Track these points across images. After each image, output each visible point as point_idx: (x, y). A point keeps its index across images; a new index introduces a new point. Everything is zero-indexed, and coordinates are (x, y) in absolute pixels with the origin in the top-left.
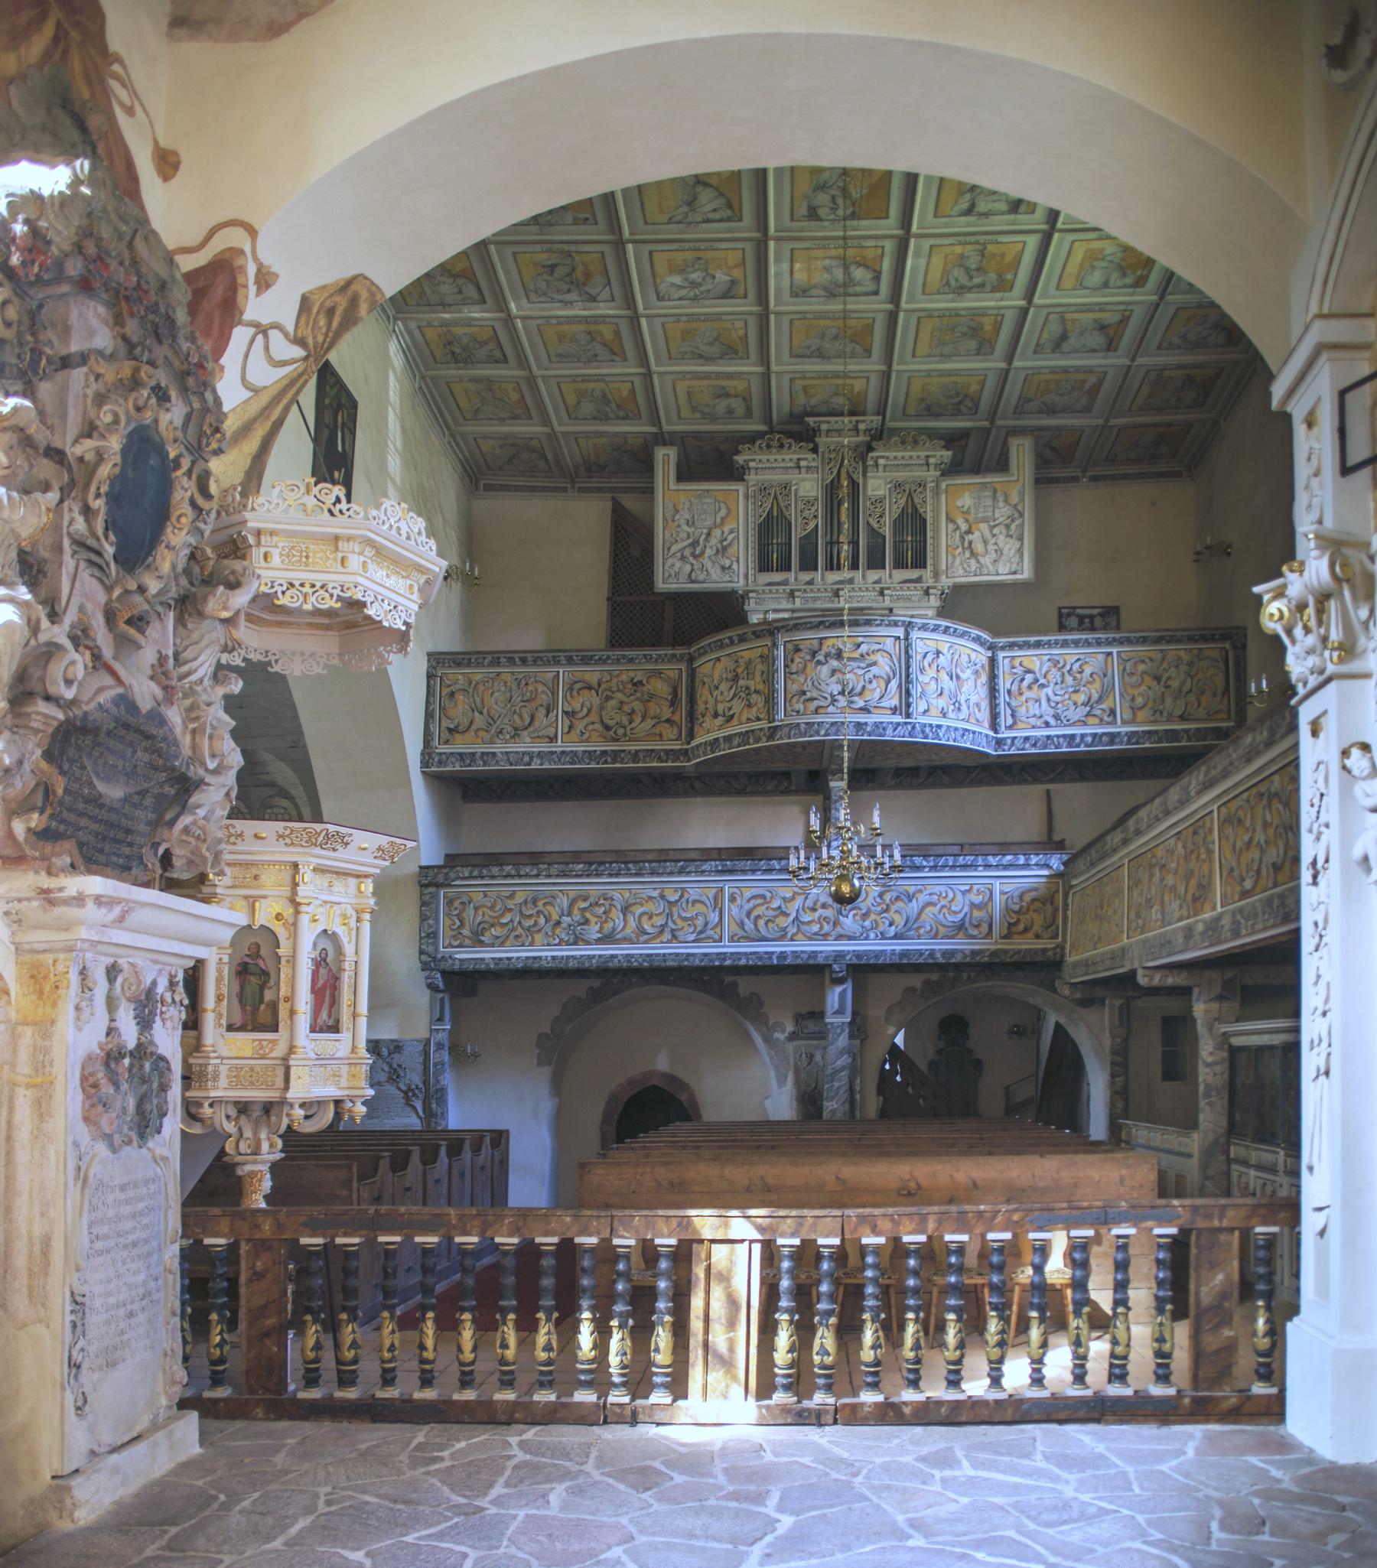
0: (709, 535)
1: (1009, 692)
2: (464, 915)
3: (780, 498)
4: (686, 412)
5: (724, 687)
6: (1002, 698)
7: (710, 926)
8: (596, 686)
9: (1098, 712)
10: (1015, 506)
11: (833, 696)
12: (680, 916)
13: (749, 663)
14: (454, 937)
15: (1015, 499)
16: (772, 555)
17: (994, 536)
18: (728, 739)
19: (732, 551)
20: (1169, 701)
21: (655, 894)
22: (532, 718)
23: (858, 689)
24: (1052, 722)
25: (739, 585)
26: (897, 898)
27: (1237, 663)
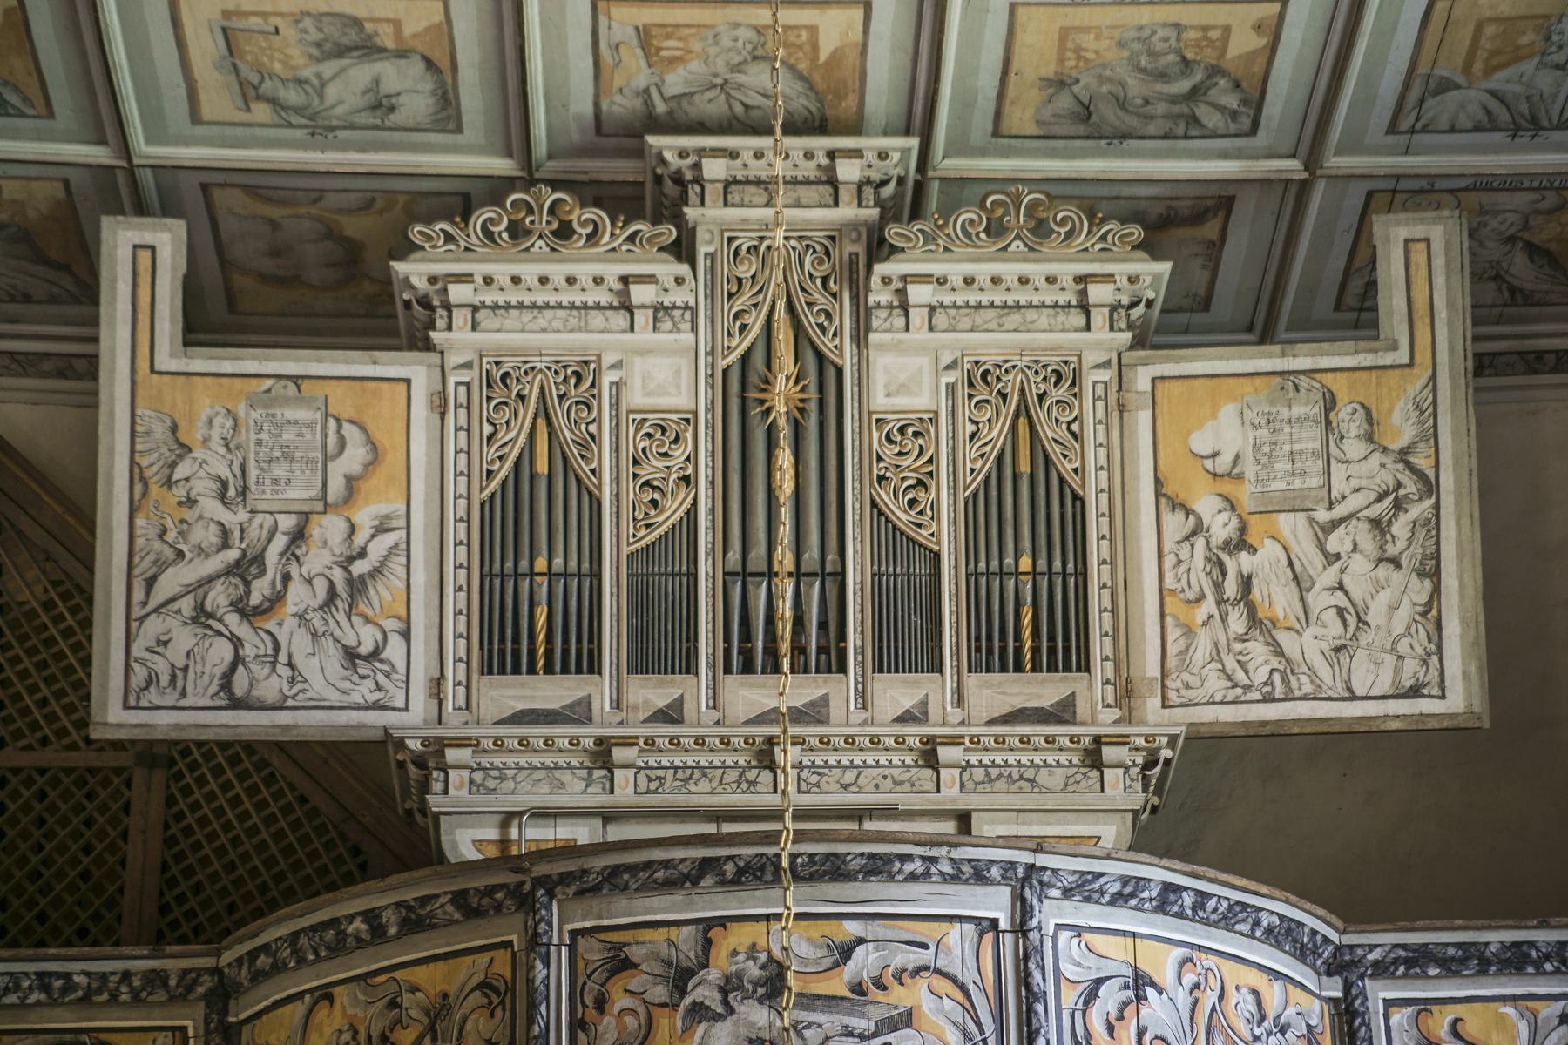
0: (299, 535)
3: (559, 412)
10: (1403, 456)
15: (1402, 428)
19: (384, 593)
25: (411, 718)
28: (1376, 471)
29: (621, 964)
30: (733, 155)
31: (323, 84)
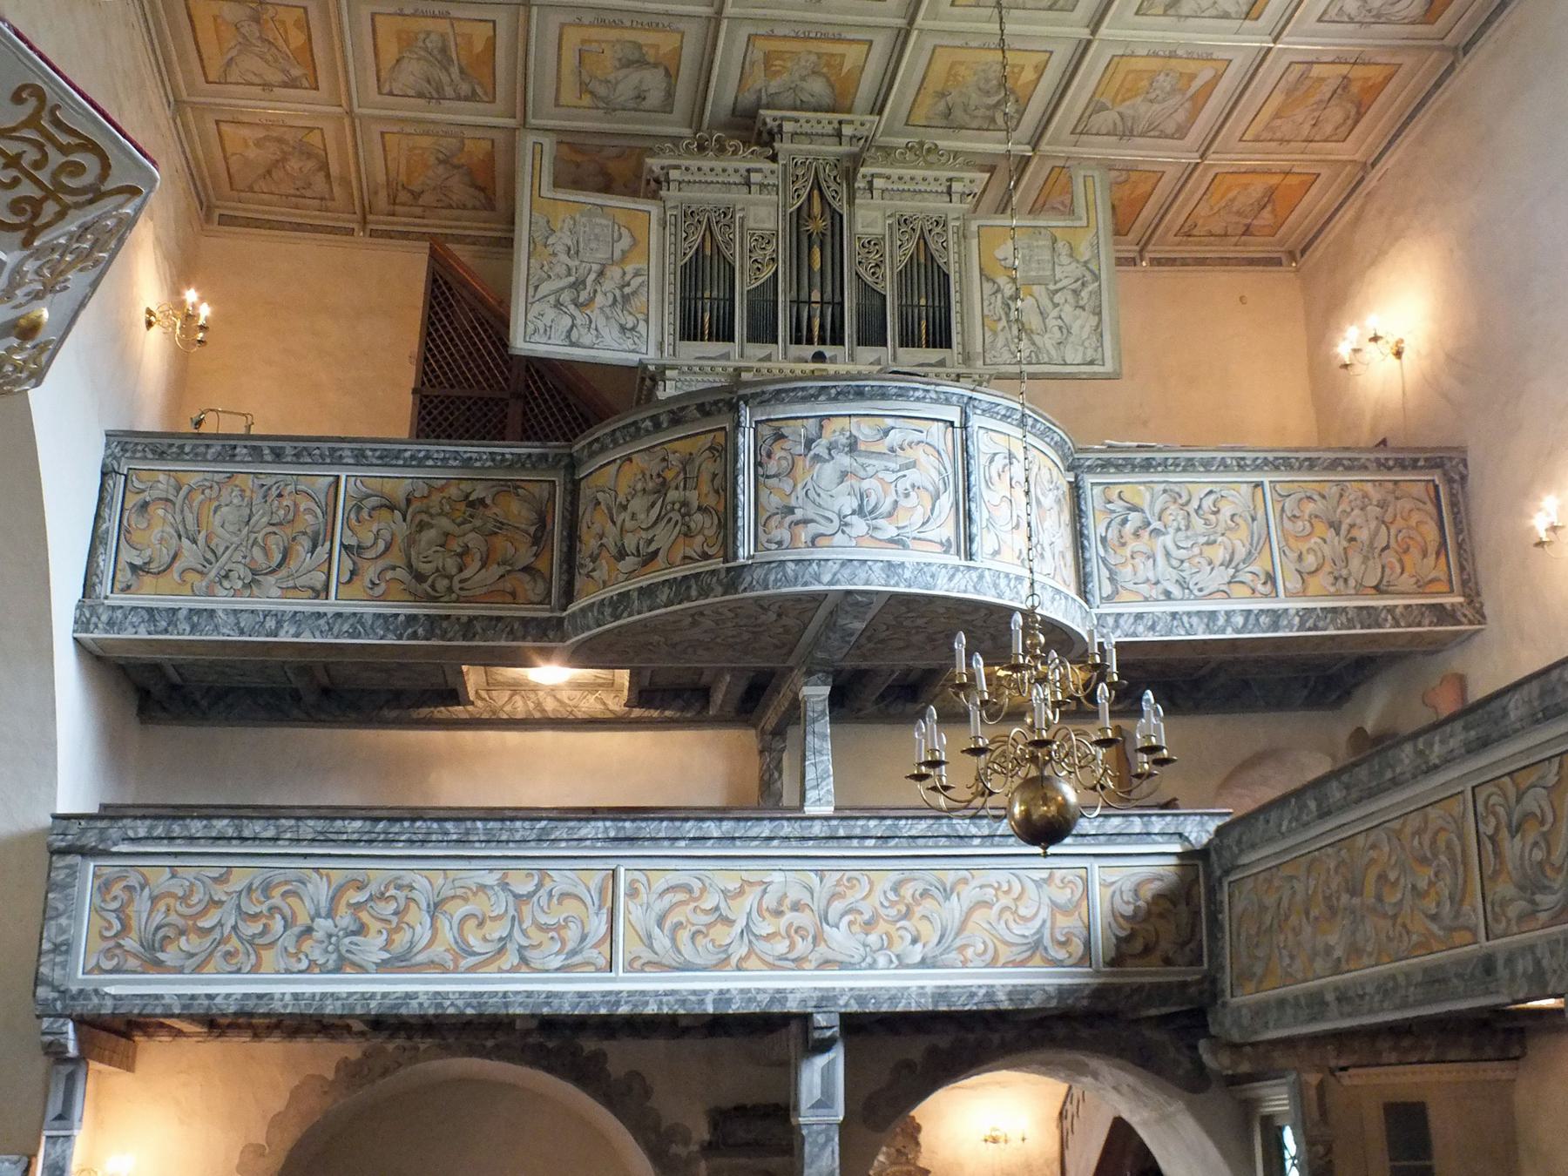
0: (601, 274)
1: (1104, 540)
2: (130, 910)
3: (716, 229)
4: (568, 96)
5: (637, 504)
6: (1094, 550)
7: (590, 941)
8: (403, 504)
9: (1248, 578)
10: (1086, 263)
11: (841, 517)
12: (535, 923)
13: (687, 462)
14: (108, 953)
15: (1085, 252)
16: (700, 320)
17: (1056, 305)
18: (647, 592)
19: (638, 302)
20: (1356, 562)
21: (491, 879)
22: (286, 555)
23: (886, 507)
24: (1176, 591)
25: (651, 356)
26: (925, 894)
27: (1454, 504)
28: (1074, 270)
29: (780, 436)
30: (797, 121)
31: (617, 83)
